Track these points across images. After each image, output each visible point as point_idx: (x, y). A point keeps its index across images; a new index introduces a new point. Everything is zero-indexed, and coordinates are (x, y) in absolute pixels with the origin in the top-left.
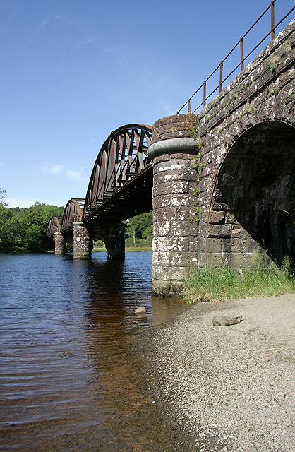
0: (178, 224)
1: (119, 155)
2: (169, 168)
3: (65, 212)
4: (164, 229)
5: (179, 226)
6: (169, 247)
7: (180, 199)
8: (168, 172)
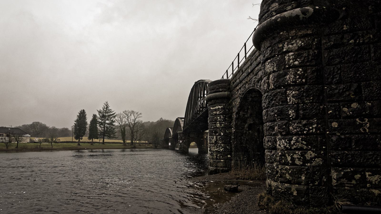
0: (220, 137)
1: (202, 94)
2: (215, 108)
4: (213, 140)
5: (220, 138)
6: (216, 149)
7: (221, 124)
8: (216, 110)
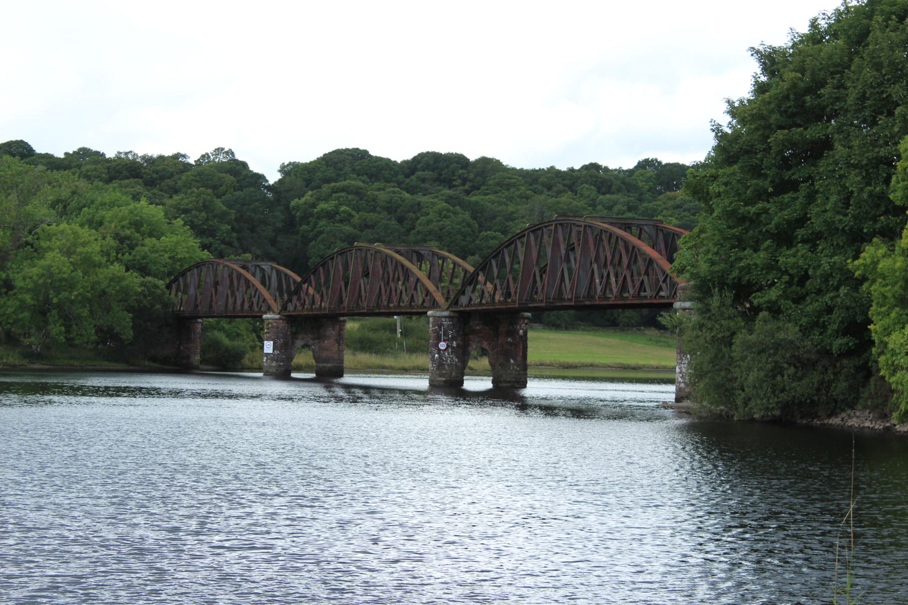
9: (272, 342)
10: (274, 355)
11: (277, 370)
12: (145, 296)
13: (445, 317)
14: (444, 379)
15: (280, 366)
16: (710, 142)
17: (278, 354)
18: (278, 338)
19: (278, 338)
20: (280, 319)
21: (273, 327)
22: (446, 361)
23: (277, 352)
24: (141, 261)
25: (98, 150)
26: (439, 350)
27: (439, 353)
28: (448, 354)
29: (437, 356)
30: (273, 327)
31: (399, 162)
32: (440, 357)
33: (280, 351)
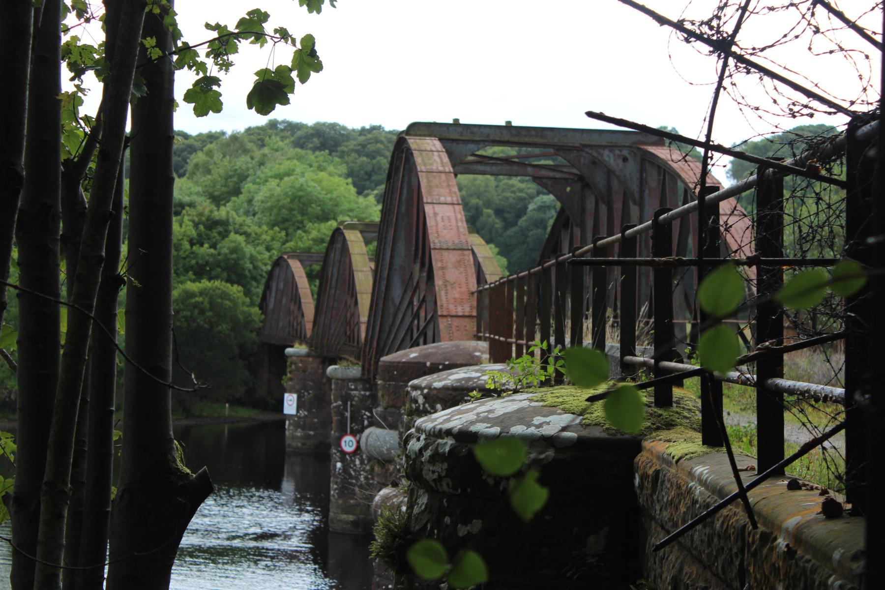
3: (268, 287)
9: (295, 396)
10: (299, 417)
11: (304, 444)
12: (202, 312)
13: (355, 380)
14: (351, 518)
15: (309, 437)
16: (714, 57)
17: (305, 416)
18: (305, 387)
19: (305, 387)
20: (308, 355)
21: (298, 369)
22: (357, 478)
23: (303, 413)
24: (229, 256)
25: (328, 118)
26: (343, 453)
27: (343, 460)
28: (362, 462)
29: (339, 465)
30: (298, 369)
31: (278, 106)
32: (345, 469)
33: (309, 411)
